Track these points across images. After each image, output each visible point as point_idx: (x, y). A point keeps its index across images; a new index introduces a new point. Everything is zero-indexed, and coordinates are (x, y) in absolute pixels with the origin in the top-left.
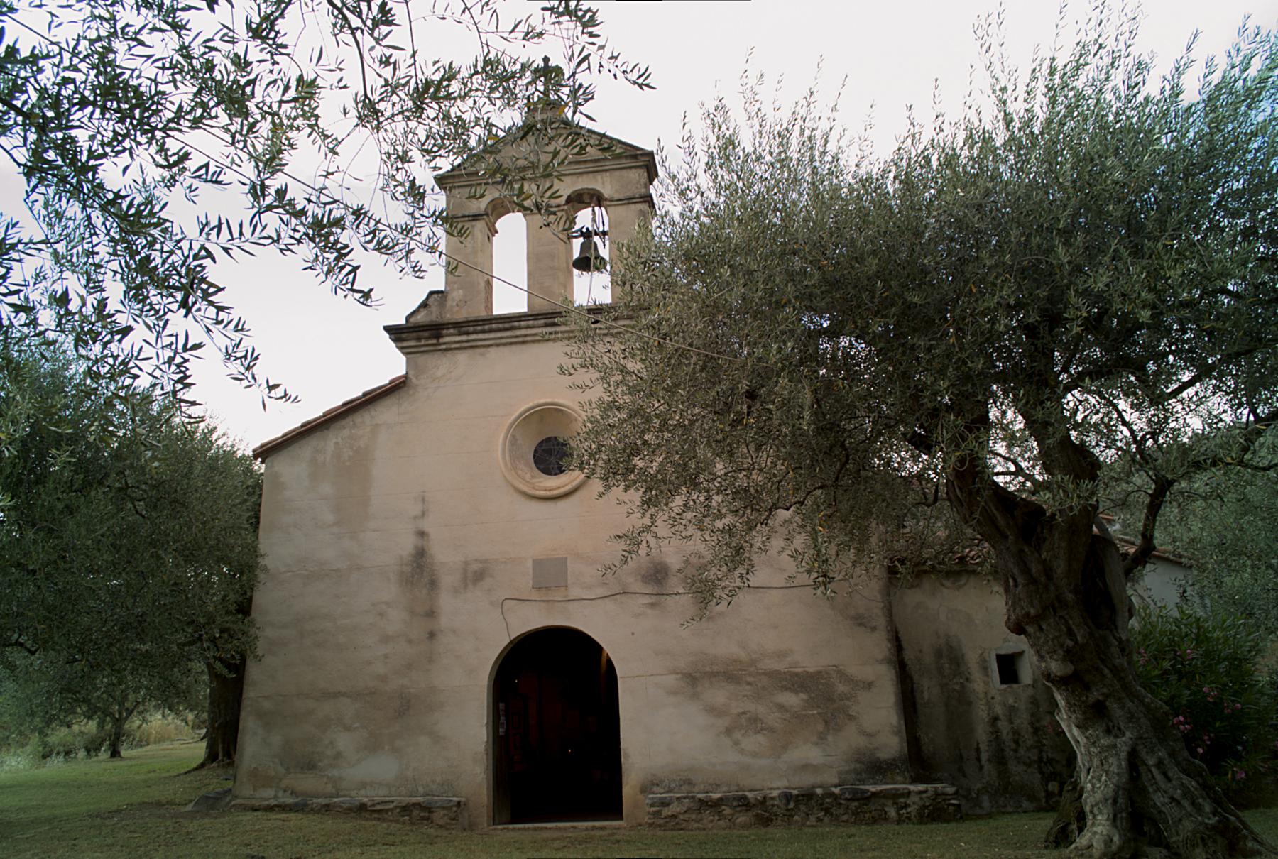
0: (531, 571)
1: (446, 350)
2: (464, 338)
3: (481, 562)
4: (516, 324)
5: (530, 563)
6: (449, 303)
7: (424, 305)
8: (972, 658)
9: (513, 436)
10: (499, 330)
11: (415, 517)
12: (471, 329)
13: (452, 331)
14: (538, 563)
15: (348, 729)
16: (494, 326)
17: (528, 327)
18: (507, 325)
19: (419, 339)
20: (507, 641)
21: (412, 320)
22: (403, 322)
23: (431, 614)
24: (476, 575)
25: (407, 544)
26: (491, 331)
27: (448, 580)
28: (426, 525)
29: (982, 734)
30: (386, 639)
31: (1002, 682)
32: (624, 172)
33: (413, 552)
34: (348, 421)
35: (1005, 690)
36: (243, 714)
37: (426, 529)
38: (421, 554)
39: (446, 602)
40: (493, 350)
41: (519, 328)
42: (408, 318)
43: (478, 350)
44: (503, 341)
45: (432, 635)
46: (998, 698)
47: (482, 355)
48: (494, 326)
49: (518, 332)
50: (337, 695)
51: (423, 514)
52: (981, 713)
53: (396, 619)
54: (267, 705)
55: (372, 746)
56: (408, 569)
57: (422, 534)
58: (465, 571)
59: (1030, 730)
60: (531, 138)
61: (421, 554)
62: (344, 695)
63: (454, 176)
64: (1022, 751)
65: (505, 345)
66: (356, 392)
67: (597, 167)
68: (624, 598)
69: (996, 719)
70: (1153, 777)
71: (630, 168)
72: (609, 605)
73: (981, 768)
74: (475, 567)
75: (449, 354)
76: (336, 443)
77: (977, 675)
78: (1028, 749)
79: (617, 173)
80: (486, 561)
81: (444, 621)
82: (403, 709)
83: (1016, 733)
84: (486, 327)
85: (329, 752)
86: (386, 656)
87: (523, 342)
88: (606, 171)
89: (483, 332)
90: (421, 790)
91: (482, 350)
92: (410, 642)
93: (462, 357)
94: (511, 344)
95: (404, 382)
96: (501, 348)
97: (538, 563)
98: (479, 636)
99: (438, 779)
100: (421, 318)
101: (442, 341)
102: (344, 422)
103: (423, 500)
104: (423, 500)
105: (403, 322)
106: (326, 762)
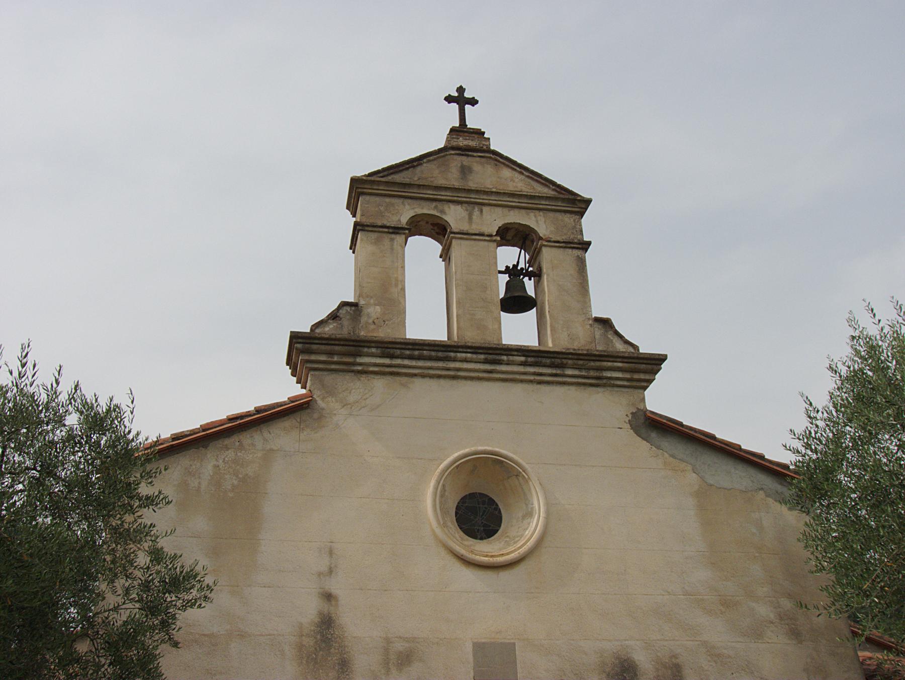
0: (471, 658)
1: (359, 372)
2: (387, 361)
3: (407, 640)
4: (452, 354)
5: (469, 648)
6: (364, 319)
7: (334, 316)
9: (444, 486)
10: (430, 359)
11: (320, 574)
12: (398, 352)
13: (374, 350)
14: (479, 648)
17: (465, 360)
18: (440, 354)
19: (331, 354)
21: (318, 331)
22: (308, 331)
25: (309, 609)
26: (419, 358)
28: (335, 586)
32: (559, 216)
33: (317, 620)
34: (234, 440)
37: (334, 591)
38: (326, 624)
40: (418, 381)
41: (455, 360)
43: (398, 378)
47: (404, 385)
49: (452, 365)
51: (331, 571)
56: (309, 642)
57: (328, 597)
58: (386, 650)
60: (353, 308)
61: (326, 624)
63: (373, 182)
65: (431, 377)
66: (748, 445)
67: (529, 202)
71: (565, 212)
74: (399, 646)
75: (363, 378)
76: (216, 466)
79: (551, 214)
80: (413, 640)
84: (416, 353)
87: (454, 378)
88: (540, 210)
89: (411, 358)
91: (404, 379)
93: (379, 384)
94: (439, 377)
95: (308, 403)
96: (427, 380)
97: (479, 648)
100: (329, 330)
101: (359, 360)
102: (227, 441)
104: (331, 552)
105: (308, 331)
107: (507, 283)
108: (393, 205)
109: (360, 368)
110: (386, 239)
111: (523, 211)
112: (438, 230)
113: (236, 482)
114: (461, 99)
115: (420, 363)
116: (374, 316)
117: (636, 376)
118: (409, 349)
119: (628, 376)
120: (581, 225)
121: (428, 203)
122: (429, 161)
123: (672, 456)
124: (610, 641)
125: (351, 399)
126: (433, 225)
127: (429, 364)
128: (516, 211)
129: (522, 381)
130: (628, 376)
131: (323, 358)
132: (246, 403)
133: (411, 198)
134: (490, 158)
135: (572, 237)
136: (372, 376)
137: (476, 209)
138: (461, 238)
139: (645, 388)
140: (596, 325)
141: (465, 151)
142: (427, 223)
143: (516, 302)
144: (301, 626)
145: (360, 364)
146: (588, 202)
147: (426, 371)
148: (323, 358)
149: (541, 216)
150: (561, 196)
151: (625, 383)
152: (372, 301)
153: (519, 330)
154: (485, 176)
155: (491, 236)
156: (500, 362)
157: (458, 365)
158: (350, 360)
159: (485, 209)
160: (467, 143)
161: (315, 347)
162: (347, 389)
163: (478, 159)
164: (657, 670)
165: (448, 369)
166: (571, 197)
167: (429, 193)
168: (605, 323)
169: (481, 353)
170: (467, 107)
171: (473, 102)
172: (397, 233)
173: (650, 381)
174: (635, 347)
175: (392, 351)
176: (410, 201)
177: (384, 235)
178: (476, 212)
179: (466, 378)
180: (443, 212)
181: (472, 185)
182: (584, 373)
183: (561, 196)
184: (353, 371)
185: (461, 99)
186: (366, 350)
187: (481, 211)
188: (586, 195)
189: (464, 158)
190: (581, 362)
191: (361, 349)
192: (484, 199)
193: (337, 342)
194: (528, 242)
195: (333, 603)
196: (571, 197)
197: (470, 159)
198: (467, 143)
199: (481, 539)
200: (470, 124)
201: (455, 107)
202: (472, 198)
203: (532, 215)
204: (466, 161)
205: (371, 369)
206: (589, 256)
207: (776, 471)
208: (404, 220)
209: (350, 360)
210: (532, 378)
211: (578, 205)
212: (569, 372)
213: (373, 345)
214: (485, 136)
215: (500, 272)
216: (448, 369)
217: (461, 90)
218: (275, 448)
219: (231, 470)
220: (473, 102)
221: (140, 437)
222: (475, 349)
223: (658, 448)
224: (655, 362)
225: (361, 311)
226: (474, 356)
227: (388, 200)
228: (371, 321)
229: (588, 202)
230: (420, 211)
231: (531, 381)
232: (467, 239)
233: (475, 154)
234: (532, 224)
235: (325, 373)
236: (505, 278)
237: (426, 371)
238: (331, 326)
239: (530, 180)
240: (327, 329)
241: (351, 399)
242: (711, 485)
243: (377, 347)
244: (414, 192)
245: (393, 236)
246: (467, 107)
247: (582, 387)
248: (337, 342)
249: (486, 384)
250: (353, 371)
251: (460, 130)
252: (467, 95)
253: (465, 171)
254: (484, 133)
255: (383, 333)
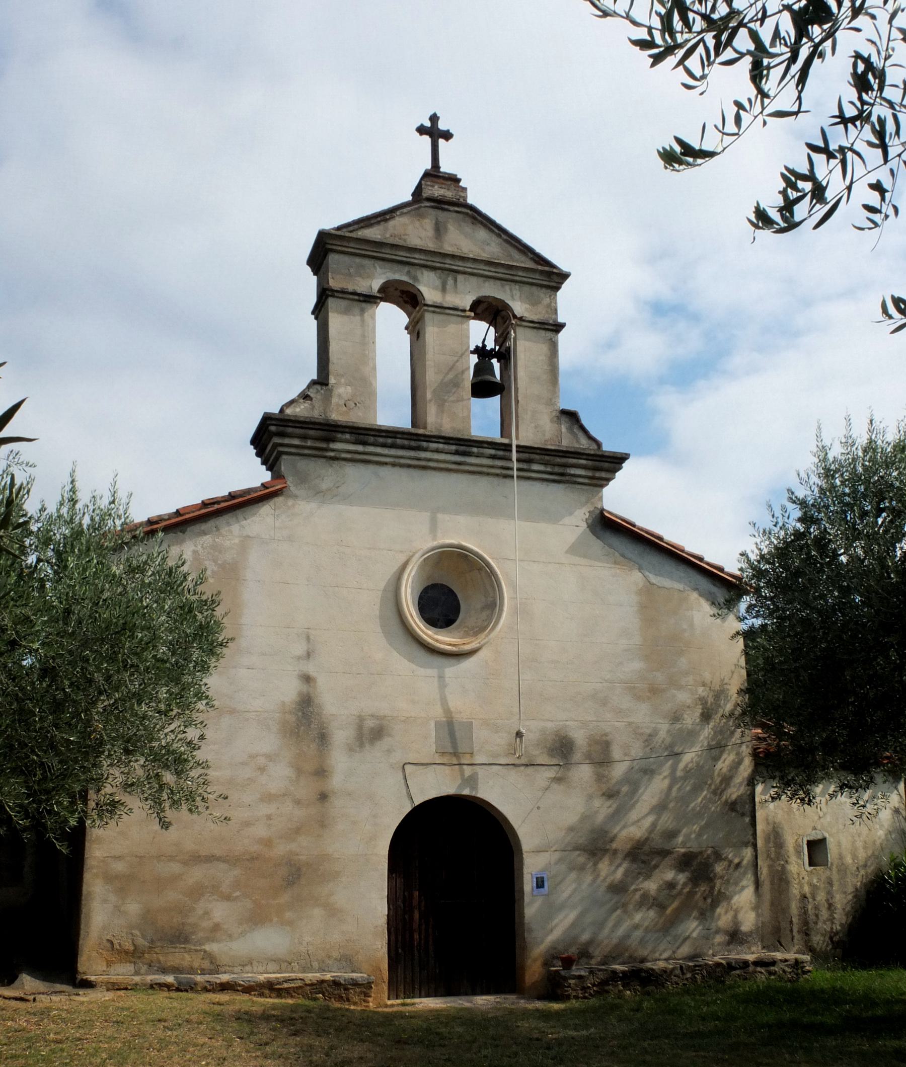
0: (433, 734)
2: (360, 448)
4: (424, 444)
5: (432, 725)
6: (335, 400)
7: (305, 396)
8: (790, 842)
10: (403, 447)
11: (299, 658)
12: (372, 439)
13: (348, 436)
15: (228, 898)
16: (399, 441)
17: (437, 451)
18: (413, 444)
19: (304, 437)
20: (408, 809)
23: (321, 773)
24: (372, 733)
25: (289, 690)
26: (393, 446)
27: (341, 736)
28: (311, 669)
29: (794, 909)
30: (268, 798)
31: (810, 865)
35: (811, 872)
36: (87, 876)
38: (306, 706)
39: (340, 761)
42: (282, 411)
44: (402, 461)
45: (323, 797)
46: (807, 878)
48: (399, 441)
49: (423, 455)
50: (211, 859)
52: (795, 891)
53: (280, 775)
54: (119, 867)
55: (257, 918)
56: (292, 718)
57: (307, 679)
59: (826, 905)
61: (306, 706)
62: (219, 859)
64: (820, 924)
65: (402, 466)
67: (505, 274)
68: (530, 770)
69: (805, 896)
70: (172, 731)
71: (542, 286)
72: (513, 774)
73: (793, 938)
74: (370, 723)
75: (336, 464)
77: (793, 859)
78: (824, 922)
79: (527, 288)
81: (336, 781)
82: (293, 879)
83: (816, 908)
85: (206, 924)
86: (269, 817)
87: (424, 468)
89: (384, 445)
90: (316, 965)
92: (298, 802)
93: (353, 472)
94: (409, 466)
96: (397, 469)
98: (375, 804)
99: (335, 954)
101: (333, 446)
102: (204, 526)
103: (308, 639)
104: (308, 639)
106: (201, 935)
107: (476, 365)
108: (363, 266)
109: (332, 454)
110: (356, 307)
111: (498, 282)
112: (408, 299)
113: (215, 569)
114: (434, 132)
115: (393, 452)
116: (346, 397)
117: (598, 474)
118: (382, 436)
119: (590, 474)
120: (556, 303)
121: (400, 266)
122: (402, 214)
123: (623, 556)
124: (552, 721)
125: (324, 486)
126: (403, 292)
127: (400, 452)
128: (492, 282)
129: (488, 474)
130: (590, 474)
131: (296, 442)
132: (220, 488)
133: (383, 259)
134: (467, 214)
135: (546, 316)
136: (344, 463)
137: (450, 278)
138: (434, 312)
139: (602, 486)
140: (564, 419)
141: (440, 204)
142: (396, 289)
143: (483, 387)
144: (283, 703)
145: (333, 450)
146: (565, 276)
147: (397, 460)
148: (296, 442)
149: (516, 290)
150: (540, 268)
151: (586, 481)
152: (343, 380)
153: (483, 418)
154: (461, 240)
155: (464, 311)
156: (469, 454)
157: (428, 455)
158: (324, 445)
159: (460, 277)
160: (439, 194)
161: (290, 430)
162: (319, 476)
163: (454, 215)
164: (590, 745)
165: (419, 459)
166: (547, 269)
167: (402, 255)
168: (571, 417)
169: (452, 444)
170: (441, 141)
171: (447, 136)
172: (369, 302)
173: (608, 480)
174: (599, 444)
175: (366, 438)
176: (381, 263)
177: (355, 303)
178: (450, 282)
179: (435, 469)
180: (415, 279)
181: (448, 248)
182: (549, 469)
183: (540, 268)
184: (325, 457)
185: (434, 132)
186: (339, 435)
187: (456, 280)
188: (564, 267)
189: (439, 212)
190: (547, 458)
191: (334, 434)
192: (458, 265)
193: (311, 426)
194: (499, 320)
195: (312, 684)
196: (547, 269)
197: (446, 214)
198: (439, 194)
199: (441, 627)
200: (446, 167)
201: (427, 139)
202: (448, 265)
203: (507, 288)
204: (442, 215)
205: (344, 455)
206: (562, 336)
207: (712, 575)
208: (376, 285)
209: (324, 445)
210: (498, 471)
211: (551, 277)
212: (535, 467)
213: (347, 430)
214: (461, 184)
215: (472, 352)
216: (419, 459)
217: (434, 118)
218: (251, 535)
219: (210, 557)
220: (447, 136)
221: (32, 468)
222: (447, 440)
223: (610, 546)
224: (616, 461)
225: (331, 391)
226: (446, 447)
227: (358, 260)
228: (342, 402)
229: (565, 276)
230: (397, 277)
231: (497, 475)
232: (439, 313)
233: (452, 208)
234: (500, 295)
235: (297, 458)
236: (474, 359)
237: (397, 460)
238: (302, 407)
239: (507, 245)
240: (298, 410)
241: (324, 486)
242: (654, 584)
243: (351, 433)
244: (387, 253)
245: (364, 305)
246: (441, 141)
247: (545, 483)
248: (311, 426)
249: (454, 477)
250: (325, 457)
251: (433, 174)
252: (442, 126)
253: (439, 230)
254: (459, 180)
255: (357, 417)
